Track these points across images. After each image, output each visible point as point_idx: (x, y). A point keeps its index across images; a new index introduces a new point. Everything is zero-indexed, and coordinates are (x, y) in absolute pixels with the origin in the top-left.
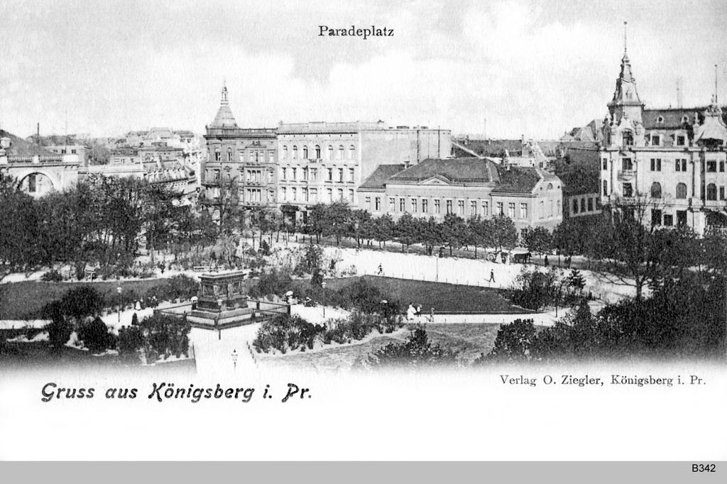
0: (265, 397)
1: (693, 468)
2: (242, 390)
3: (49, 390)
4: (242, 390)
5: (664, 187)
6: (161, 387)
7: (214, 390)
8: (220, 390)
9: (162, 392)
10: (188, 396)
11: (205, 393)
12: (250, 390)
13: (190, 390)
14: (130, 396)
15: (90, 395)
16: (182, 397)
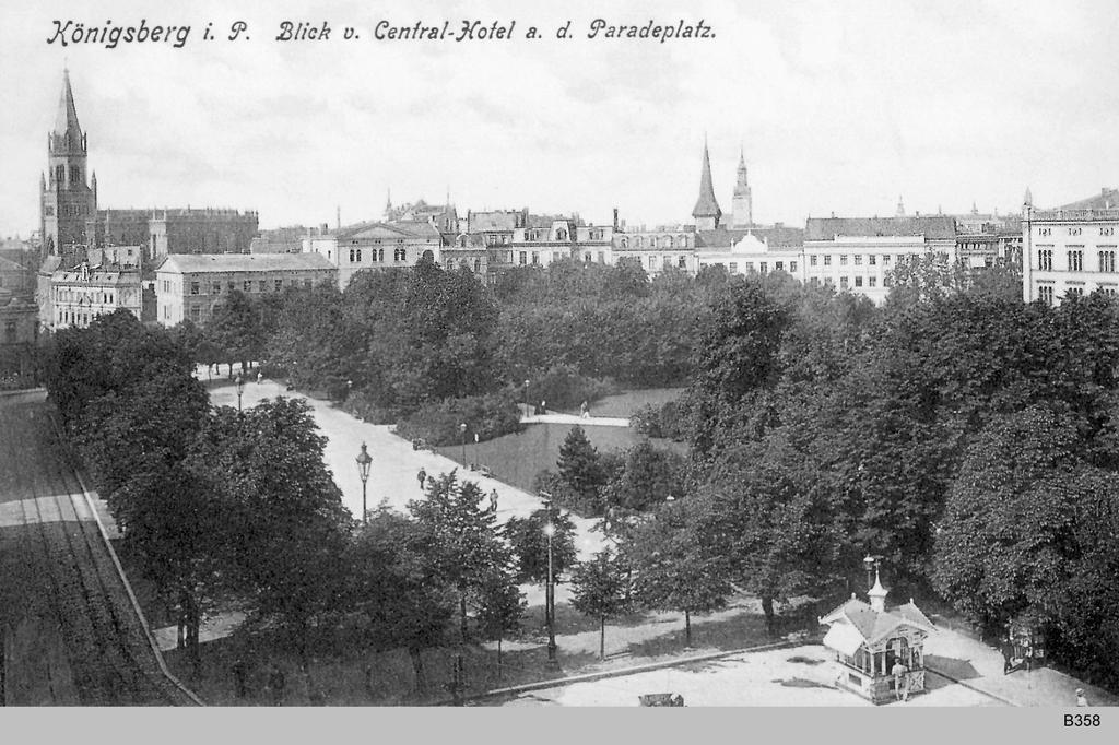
0: (205, 38)
1: (1066, 720)
2: (175, 29)
3: (381, 31)
4: (175, 29)
5: (1000, 668)
6: (475, 24)
7: (137, 31)
8: (147, 29)
9: (475, 34)
10: (102, 41)
11: (124, 33)
12: (183, 28)
13: (105, 30)
14: (125, 38)
15: (129, 38)
16: (407, 37)
